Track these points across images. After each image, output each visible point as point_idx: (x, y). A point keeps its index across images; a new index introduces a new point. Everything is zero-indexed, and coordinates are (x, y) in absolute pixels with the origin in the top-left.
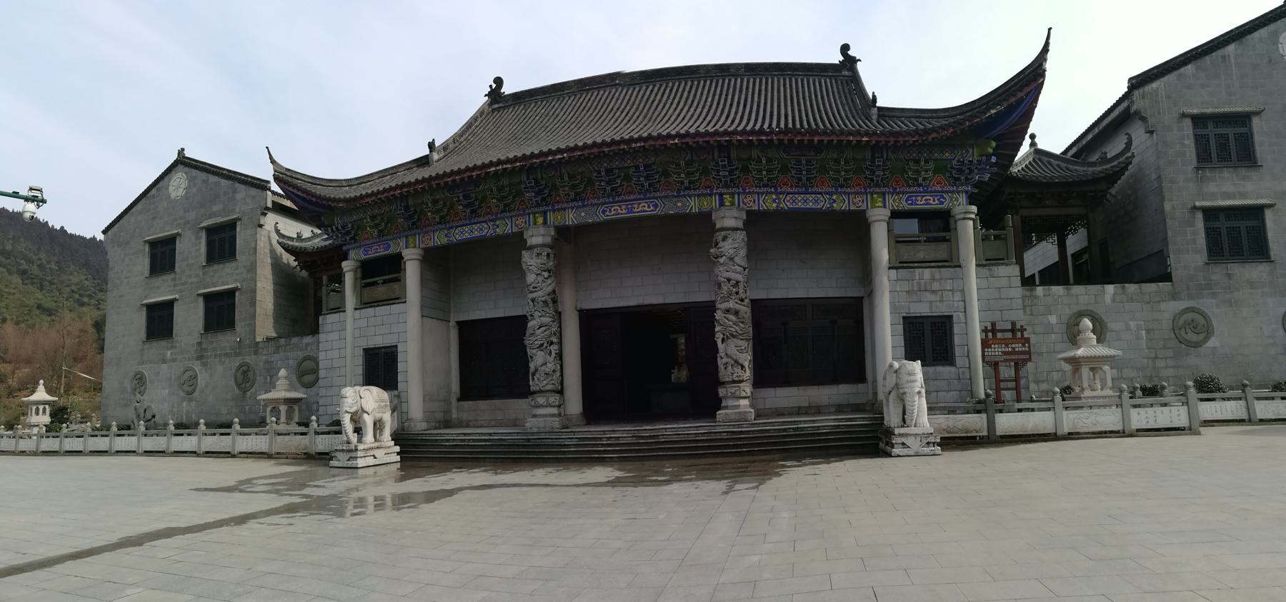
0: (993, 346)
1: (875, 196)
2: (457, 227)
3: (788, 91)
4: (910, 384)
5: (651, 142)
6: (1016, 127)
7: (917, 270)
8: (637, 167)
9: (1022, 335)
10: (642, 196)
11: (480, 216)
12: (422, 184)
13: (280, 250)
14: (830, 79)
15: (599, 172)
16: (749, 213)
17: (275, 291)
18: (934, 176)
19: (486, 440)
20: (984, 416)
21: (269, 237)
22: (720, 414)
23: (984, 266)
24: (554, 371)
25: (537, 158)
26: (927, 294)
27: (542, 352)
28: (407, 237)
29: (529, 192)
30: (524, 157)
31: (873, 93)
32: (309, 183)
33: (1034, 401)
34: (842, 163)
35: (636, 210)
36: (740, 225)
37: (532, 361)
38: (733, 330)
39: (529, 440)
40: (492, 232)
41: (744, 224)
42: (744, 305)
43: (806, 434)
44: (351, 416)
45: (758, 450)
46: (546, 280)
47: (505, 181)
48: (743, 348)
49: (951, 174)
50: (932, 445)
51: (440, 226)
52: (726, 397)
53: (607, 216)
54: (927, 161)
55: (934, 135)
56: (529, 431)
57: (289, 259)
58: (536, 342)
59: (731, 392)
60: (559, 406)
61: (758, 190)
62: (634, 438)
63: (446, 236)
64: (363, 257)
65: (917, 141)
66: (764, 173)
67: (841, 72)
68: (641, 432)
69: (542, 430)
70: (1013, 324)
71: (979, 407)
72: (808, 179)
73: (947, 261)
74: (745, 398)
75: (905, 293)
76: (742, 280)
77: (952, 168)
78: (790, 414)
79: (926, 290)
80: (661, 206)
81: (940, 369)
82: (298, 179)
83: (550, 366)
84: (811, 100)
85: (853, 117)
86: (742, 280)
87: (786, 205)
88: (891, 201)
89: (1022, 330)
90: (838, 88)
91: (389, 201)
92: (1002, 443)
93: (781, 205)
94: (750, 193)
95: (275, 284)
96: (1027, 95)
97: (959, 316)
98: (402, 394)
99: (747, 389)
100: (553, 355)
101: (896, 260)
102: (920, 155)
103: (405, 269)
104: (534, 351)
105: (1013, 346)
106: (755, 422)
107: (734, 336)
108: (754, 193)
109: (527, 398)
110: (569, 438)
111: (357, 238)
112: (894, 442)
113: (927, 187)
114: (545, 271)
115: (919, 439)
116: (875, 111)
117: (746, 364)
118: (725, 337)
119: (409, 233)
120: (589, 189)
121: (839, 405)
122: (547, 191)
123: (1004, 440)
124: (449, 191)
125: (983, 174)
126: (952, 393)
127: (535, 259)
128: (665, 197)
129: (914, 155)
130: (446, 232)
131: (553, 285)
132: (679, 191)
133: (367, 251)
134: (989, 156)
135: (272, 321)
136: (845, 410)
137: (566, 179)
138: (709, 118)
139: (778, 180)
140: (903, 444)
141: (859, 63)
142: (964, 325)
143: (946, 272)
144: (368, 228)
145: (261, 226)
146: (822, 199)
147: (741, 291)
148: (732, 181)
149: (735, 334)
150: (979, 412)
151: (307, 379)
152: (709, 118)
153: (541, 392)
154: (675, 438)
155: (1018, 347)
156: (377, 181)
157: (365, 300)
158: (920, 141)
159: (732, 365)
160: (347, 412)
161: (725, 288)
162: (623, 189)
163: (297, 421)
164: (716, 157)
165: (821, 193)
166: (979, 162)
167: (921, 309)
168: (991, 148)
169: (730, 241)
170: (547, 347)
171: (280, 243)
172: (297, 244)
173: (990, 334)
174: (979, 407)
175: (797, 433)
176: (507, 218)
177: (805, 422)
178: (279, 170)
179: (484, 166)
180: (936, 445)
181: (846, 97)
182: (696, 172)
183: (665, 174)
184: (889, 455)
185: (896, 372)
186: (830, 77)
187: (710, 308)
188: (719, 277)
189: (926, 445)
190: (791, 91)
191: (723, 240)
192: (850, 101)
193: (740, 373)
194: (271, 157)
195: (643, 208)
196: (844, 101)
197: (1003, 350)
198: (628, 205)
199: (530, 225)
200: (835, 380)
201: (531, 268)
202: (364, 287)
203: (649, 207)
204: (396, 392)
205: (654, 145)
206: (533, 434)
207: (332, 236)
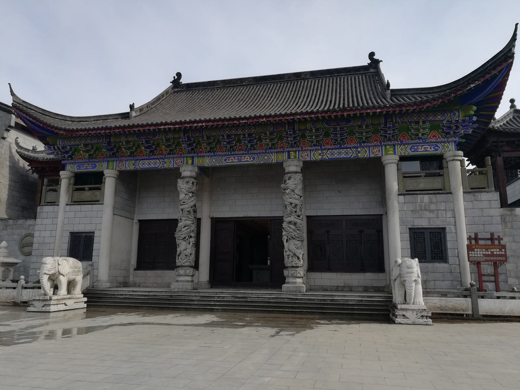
0: (476, 250)
1: (388, 147)
2: (141, 160)
3: (335, 86)
4: (408, 275)
5: (251, 121)
6: (491, 96)
7: (419, 196)
8: (244, 135)
9: (499, 243)
10: (246, 152)
11: (155, 155)
12: (119, 130)
13: (17, 157)
14: (362, 75)
15: (223, 136)
16: (305, 163)
17: (10, 186)
18: (430, 132)
19: (145, 296)
20: (469, 300)
21: (10, 147)
22: (284, 287)
23: (470, 193)
24: (191, 254)
25: (188, 124)
26: (427, 212)
27: (185, 242)
28: (108, 162)
29: (184, 144)
30: (181, 123)
31: (388, 81)
32: (40, 113)
33: (515, 292)
34: (364, 127)
35: (243, 160)
36: (299, 170)
37: (179, 247)
38: (293, 234)
39: (171, 296)
40: (162, 166)
41: (301, 170)
42: (299, 219)
43: (339, 304)
44: (49, 277)
45: (306, 312)
46: (190, 198)
47: (171, 136)
48: (299, 246)
49: (443, 130)
50: (425, 318)
51: (130, 158)
52: (288, 276)
53: (227, 162)
54: (424, 122)
55: (428, 105)
56: (172, 290)
57: (24, 164)
58: (182, 236)
59: (291, 274)
60: (193, 276)
61: (310, 148)
62: (233, 298)
63: (133, 164)
64: (77, 171)
65: (416, 109)
66: (314, 137)
67: (369, 70)
68: (238, 294)
69: (180, 290)
70: (492, 234)
71: (465, 293)
72: (342, 140)
73: (441, 190)
74: (300, 277)
75: (410, 212)
76: (299, 204)
77: (443, 126)
78: (331, 290)
79: (426, 210)
80: (257, 158)
81: (437, 265)
82: (32, 110)
83: (189, 251)
84: (348, 90)
85: (375, 98)
86: (299, 204)
87: (327, 157)
88: (399, 150)
89: (499, 239)
90: (366, 81)
91: (98, 136)
92: (484, 320)
93: (324, 157)
94: (305, 150)
95: (11, 180)
96: (499, 72)
97: (450, 228)
98: (95, 264)
99: (301, 272)
100: (191, 244)
101: (404, 190)
102: (419, 118)
103: (105, 183)
104: (180, 241)
105: (492, 250)
106: (306, 293)
107: (293, 238)
108: (307, 150)
109: (174, 270)
110: (195, 296)
111: (73, 156)
112: (397, 314)
113: (425, 139)
114: (190, 193)
115: (416, 313)
116: (389, 92)
117: (301, 256)
118: (288, 239)
119: (109, 159)
120: (218, 146)
121: (365, 287)
122: (195, 145)
123: (485, 318)
124: (137, 137)
125: (467, 129)
126: (446, 282)
127: (185, 185)
128: (259, 153)
129: (415, 119)
130: (134, 162)
131: (195, 201)
132: (266, 150)
133: (80, 167)
134: (471, 117)
135: (5, 207)
136: (369, 290)
137: (205, 138)
138: (286, 106)
139: (322, 142)
140: (404, 315)
141: (381, 63)
142: (455, 234)
143: (441, 197)
144: (81, 152)
145: (4, 138)
146: (350, 151)
147: (298, 210)
148: (295, 143)
149: (294, 237)
150: (465, 296)
151: (26, 249)
152: (286, 106)
153: (182, 266)
154: (257, 299)
155: (496, 252)
156: (93, 122)
157: (75, 199)
158: (418, 110)
159: (292, 256)
160: (46, 274)
161: (289, 208)
162: (237, 147)
163: (11, 278)
164: (287, 129)
165: (350, 148)
166: (464, 121)
167: (422, 223)
168: (473, 111)
169: (292, 180)
170: (188, 239)
171: (18, 153)
172: (32, 154)
173: (473, 242)
174: (465, 293)
175: (333, 303)
176: (171, 158)
177: (339, 296)
178: (17, 101)
179: (157, 125)
180: (428, 318)
181: (371, 86)
182: (276, 138)
183: (260, 139)
184: (393, 322)
185: (399, 266)
186: (362, 74)
187: (280, 220)
188: (286, 202)
189: (421, 318)
190: (336, 86)
191: (289, 179)
192: (374, 88)
193: (297, 262)
194: (11, 91)
195: (247, 160)
196: (370, 89)
197: (484, 253)
198: (238, 157)
199: (184, 164)
200: (362, 269)
201: (182, 190)
202: (75, 190)
203: (250, 159)
204: (90, 262)
205: (253, 122)
206: (174, 292)
207: (54, 153)
